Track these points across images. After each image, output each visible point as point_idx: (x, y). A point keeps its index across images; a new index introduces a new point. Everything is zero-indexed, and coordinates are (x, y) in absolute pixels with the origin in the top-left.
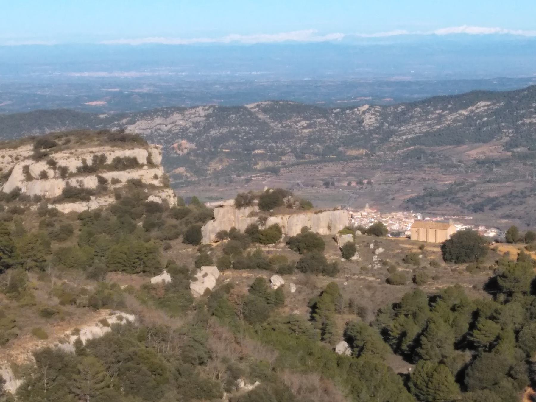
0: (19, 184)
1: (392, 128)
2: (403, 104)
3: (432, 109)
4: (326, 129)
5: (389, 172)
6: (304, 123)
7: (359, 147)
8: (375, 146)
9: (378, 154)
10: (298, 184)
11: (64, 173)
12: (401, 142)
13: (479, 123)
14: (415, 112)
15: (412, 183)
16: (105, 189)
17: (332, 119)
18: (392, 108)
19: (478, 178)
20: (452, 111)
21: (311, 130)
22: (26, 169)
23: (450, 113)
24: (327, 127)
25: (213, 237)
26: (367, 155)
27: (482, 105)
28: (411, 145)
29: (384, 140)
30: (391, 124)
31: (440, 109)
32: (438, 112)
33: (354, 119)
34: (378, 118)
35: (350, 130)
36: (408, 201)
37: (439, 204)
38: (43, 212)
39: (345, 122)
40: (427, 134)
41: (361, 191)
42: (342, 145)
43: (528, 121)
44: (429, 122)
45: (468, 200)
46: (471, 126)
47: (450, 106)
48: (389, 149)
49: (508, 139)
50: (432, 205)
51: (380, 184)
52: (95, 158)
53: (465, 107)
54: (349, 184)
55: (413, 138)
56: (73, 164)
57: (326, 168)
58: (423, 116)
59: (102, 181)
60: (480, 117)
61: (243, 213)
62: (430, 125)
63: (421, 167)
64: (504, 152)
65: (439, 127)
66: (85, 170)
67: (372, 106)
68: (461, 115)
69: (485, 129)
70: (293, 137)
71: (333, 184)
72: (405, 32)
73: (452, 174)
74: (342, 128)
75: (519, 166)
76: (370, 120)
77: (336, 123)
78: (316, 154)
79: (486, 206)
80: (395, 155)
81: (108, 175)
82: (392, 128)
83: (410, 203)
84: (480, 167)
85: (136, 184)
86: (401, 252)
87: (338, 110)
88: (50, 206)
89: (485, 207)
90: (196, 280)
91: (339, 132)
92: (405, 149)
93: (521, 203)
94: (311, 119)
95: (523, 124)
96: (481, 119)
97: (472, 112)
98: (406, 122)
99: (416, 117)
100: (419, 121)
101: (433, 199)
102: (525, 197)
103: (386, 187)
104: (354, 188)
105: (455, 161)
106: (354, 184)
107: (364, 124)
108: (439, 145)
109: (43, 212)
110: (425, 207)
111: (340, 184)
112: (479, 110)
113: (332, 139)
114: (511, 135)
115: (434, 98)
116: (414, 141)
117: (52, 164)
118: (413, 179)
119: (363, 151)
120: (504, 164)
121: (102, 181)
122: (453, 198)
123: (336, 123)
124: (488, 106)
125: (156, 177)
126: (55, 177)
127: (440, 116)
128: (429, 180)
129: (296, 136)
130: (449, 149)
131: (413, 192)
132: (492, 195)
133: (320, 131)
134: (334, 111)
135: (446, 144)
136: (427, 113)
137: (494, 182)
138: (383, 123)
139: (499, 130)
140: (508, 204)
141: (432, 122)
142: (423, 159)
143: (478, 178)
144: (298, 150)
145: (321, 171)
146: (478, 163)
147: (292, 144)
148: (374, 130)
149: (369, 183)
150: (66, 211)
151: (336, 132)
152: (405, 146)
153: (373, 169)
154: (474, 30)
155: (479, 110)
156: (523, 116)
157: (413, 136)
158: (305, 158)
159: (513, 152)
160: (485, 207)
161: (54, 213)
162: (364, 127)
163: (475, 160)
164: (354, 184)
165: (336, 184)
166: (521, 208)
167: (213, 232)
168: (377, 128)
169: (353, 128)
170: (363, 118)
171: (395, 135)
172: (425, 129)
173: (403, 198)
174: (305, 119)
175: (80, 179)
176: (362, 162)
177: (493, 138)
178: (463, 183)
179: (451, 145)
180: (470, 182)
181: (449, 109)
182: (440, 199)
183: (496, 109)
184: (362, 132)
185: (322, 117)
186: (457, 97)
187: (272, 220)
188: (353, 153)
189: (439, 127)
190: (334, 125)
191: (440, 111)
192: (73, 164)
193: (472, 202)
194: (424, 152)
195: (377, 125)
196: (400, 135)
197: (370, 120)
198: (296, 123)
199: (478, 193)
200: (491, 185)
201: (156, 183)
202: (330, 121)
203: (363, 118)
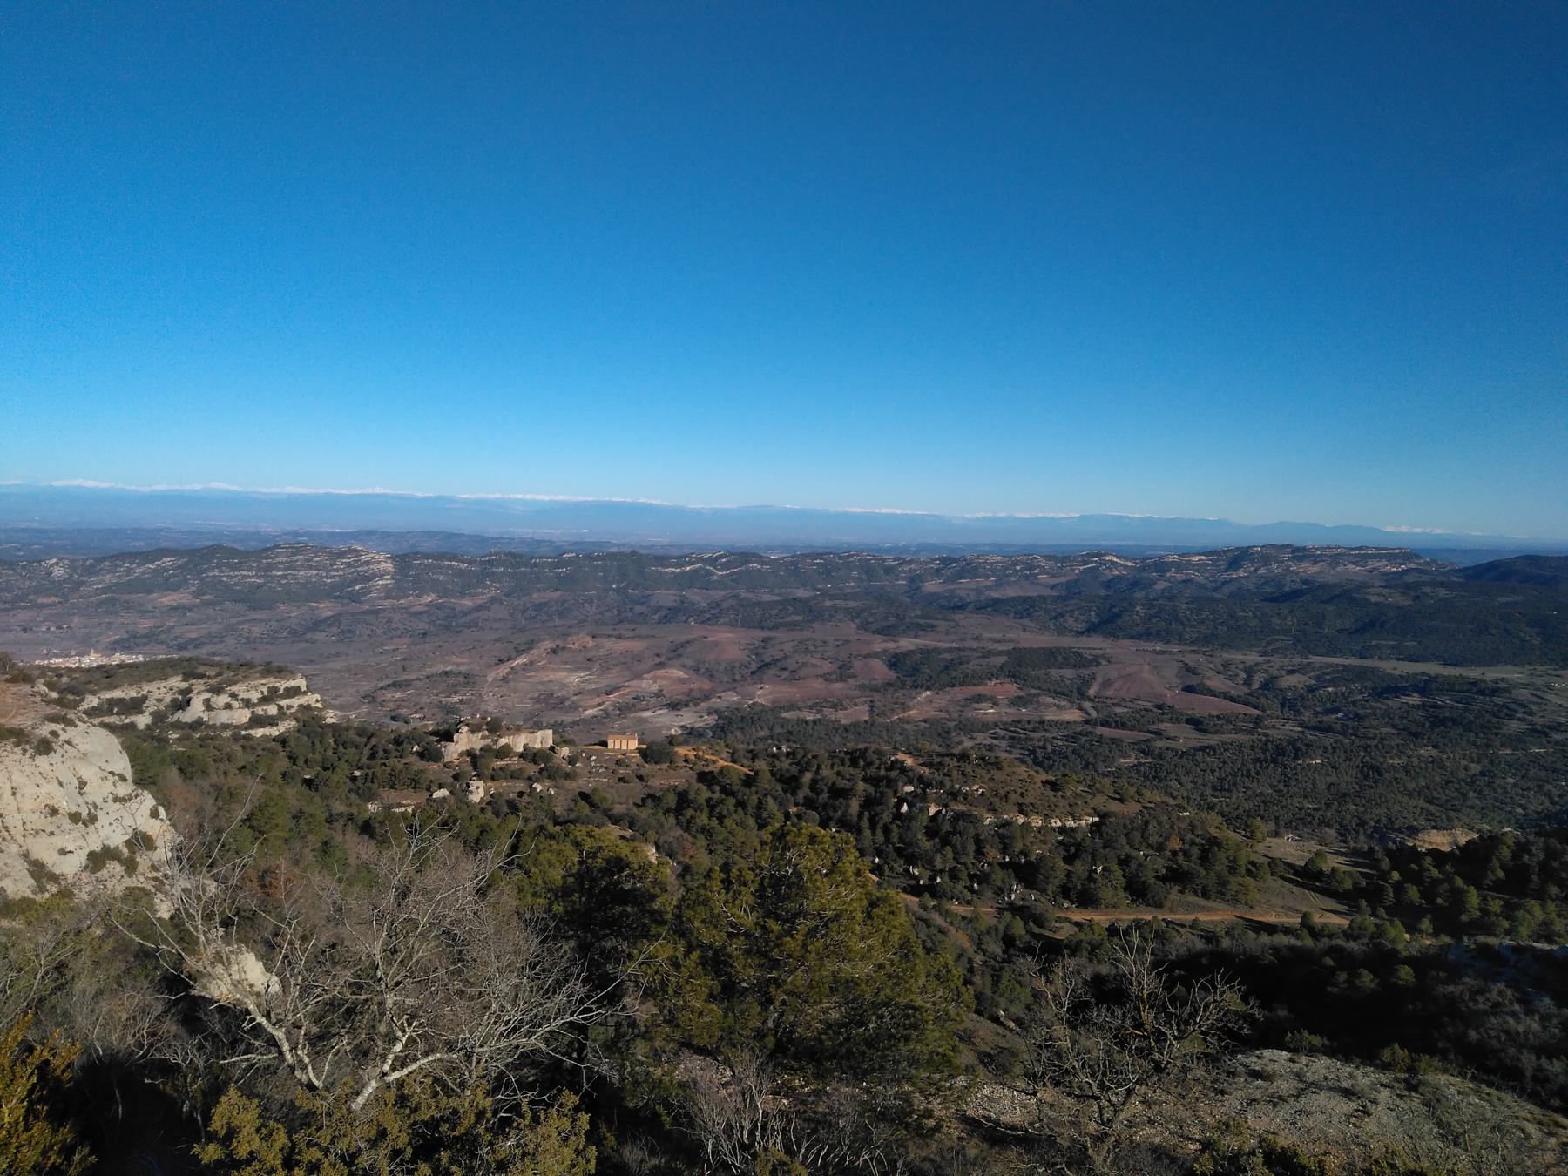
0: (201, 714)
1: (82, 578)
7: (50, 595)
11: (247, 703)
16: (284, 714)
20: (139, 565)
27: (167, 561)
28: (102, 593)
37: (145, 645)
38: (236, 738)
40: (116, 584)
41: (62, 635)
48: (81, 597)
54: (48, 629)
56: (255, 696)
59: (280, 708)
62: (119, 577)
63: (117, 613)
66: (264, 700)
67: (61, 559)
71: (31, 629)
75: (210, 611)
76: (59, 572)
81: (284, 703)
82: (82, 578)
85: (306, 708)
88: (243, 733)
91: (27, 583)
93: (221, 642)
97: (158, 565)
98: (97, 573)
101: (137, 641)
104: (54, 632)
105: (150, 608)
106: (52, 629)
109: (236, 738)
116: (105, 590)
119: (56, 600)
120: (195, 609)
121: (280, 708)
125: (317, 701)
132: (193, 636)
136: (117, 566)
138: (72, 575)
139: (186, 581)
149: (69, 627)
150: (258, 736)
152: (97, 595)
154: (90, 484)
156: (206, 570)
161: (249, 738)
166: (222, 645)
178: (161, 626)
182: (145, 640)
187: (503, 741)
188: (46, 600)
192: (255, 696)
197: (59, 572)
201: (319, 705)
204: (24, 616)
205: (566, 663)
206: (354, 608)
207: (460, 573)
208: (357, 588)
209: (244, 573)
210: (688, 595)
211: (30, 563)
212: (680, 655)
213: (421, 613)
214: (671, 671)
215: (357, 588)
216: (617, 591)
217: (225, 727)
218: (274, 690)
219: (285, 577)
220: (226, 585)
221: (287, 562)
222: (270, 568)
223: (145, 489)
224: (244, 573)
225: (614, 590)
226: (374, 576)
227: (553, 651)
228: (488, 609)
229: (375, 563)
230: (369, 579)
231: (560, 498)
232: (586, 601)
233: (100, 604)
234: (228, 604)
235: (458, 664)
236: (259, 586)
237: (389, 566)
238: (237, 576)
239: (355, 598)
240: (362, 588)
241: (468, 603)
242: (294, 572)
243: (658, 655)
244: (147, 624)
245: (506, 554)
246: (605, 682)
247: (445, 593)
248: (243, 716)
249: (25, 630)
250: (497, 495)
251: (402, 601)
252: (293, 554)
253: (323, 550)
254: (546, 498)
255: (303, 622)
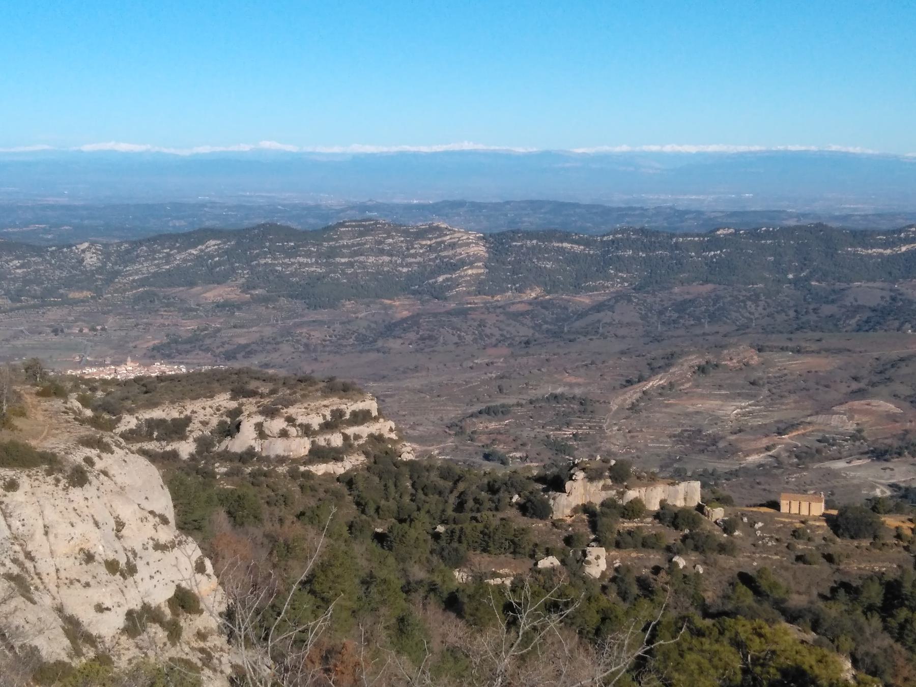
0: (253, 443)
2: (126, 242)
3: (159, 248)
4: (42, 269)
5: (122, 317)
6: (17, 263)
7: (81, 289)
8: (100, 288)
9: (105, 296)
10: (22, 331)
11: (306, 430)
12: (128, 283)
13: (211, 263)
14: (141, 250)
15: (151, 330)
16: (351, 446)
17: (48, 258)
18: (115, 246)
19: (221, 323)
21: (25, 270)
22: (259, 427)
23: (179, 252)
24: (43, 267)
25: (568, 511)
26: (92, 298)
27: (212, 244)
28: (139, 287)
29: (109, 281)
30: (115, 264)
31: (168, 248)
32: (165, 251)
33: (72, 258)
34: (100, 257)
35: (69, 270)
36: (153, 349)
37: (187, 352)
38: (293, 474)
39: (62, 260)
40: (155, 275)
42: (62, 286)
43: (263, 262)
44: (156, 262)
45: (218, 347)
46: (203, 266)
47: (178, 245)
48: (116, 291)
49: (243, 280)
50: (180, 354)
51: (115, 330)
52: (333, 413)
53: (194, 246)
54: (81, 331)
55: (141, 279)
56: (316, 421)
57: (50, 313)
58: (149, 255)
59: (346, 438)
60: (211, 257)
61: (597, 487)
62: (158, 266)
64: (242, 294)
65: (168, 267)
66: (327, 427)
67: (93, 244)
68: (190, 254)
69: (218, 269)
70: (6, 278)
71: (62, 331)
72: (46, 147)
73: (192, 319)
74: (61, 267)
75: (261, 309)
77: (53, 262)
78: (34, 297)
79: (239, 353)
80: (124, 298)
81: (351, 431)
82: (117, 268)
83: (155, 351)
84: (221, 311)
86: (784, 527)
87: (54, 248)
89: (237, 355)
90: (589, 563)
91: (57, 272)
92: (134, 291)
93: (276, 350)
94: (24, 258)
95: (258, 265)
96: (212, 259)
97: (201, 251)
98: (133, 261)
99: (142, 256)
100: (146, 260)
102: (277, 343)
103: (123, 333)
104: (86, 335)
106: (86, 331)
107: (84, 264)
108: (169, 286)
109: (293, 474)
110: (173, 355)
111: (69, 331)
112: (209, 249)
113: (50, 279)
114: (247, 276)
115: (160, 236)
116: (143, 282)
117: (290, 420)
118: (151, 324)
119: (87, 294)
120: (244, 308)
122: (202, 346)
123: (53, 262)
124: (218, 245)
126: (297, 436)
127: (168, 255)
128: (168, 325)
129: (8, 276)
130: (183, 291)
131: (154, 339)
132: (243, 341)
133: (37, 271)
134: (50, 249)
135: (179, 286)
136: (154, 252)
137: (242, 327)
138: (105, 263)
139: (234, 270)
140: (261, 351)
141: (160, 261)
142: (157, 302)
143: (221, 323)
144: (13, 292)
145: (45, 316)
146: (218, 306)
147: (5, 286)
148: (96, 270)
149: (103, 329)
150: (320, 473)
151: (54, 272)
152: (132, 288)
153: (104, 313)
154: (123, 147)
155: (209, 249)
156: (257, 256)
157: (141, 276)
158: (21, 301)
159: (252, 294)
160: (237, 355)
161: (308, 475)
162: (85, 267)
163: (213, 302)
164: (86, 331)
165: (66, 330)
167: (567, 506)
168: (100, 268)
169: (73, 268)
170: (83, 258)
171: (120, 276)
172: (153, 270)
173: (145, 346)
174: (18, 258)
175: (328, 437)
176: (89, 306)
177: (228, 279)
178: (206, 329)
179: (183, 286)
180: (214, 328)
181: (178, 248)
182: (188, 347)
183: (228, 248)
184: (83, 273)
185: (36, 256)
186: (184, 235)
187: (632, 494)
188: (75, 295)
189: (168, 267)
190: (51, 264)
191: (168, 250)
192: (316, 421)
193: (221, 349)
194: (155, 295)
195: (100, 264)
196: (126, 276)
197: (91, 260)
198: (7, 262)
199: (226, 339)
200: (238, 331)
202: (46, 260)
203: (83, 258)
204: (54, 314)
205: (720, 387)
206: (435, 305)
207: (574, 258)
208: (440, 279)
209: (301, 260)
210: (903, 290)
211: (60, 248)
212: (889, 379)
213: (523, 314)
214: (874, 402)
215: (440, 279)
216: (795, 282)
217: (281, 460)
218: (338, 414)
219: (351, 264)
220: (280, 276)
221: (353, 245)
222: (333, 253)
223: (185, 153)
224: (301, 260)
225: (790, 282)
226: (462, 263)
227: (702, 370)
228: (611, 309)
229: (461, 246)
230: (454, 267)
231: (712, 148)
232: (749, 299)
233: (138, 299)
234: (283, 301)
235: (571, 385)
236: (320, 278)
237: (480, 250)
238: (293, 264)
239: (438, 293)
240: (447, 280)
241: (584, 300)
242: (362, 258)
243: (855, 379)
244: (189, 326)
245: (636, 232)
246: (777, 416)
247: (552, 286)
248: (301, 447)
249: (55, 332)
250: (625, 148)
251: (498, 297)
252: (361, 234)
253: (398, 228)
254: (692, 149)
255: (373, 325)
